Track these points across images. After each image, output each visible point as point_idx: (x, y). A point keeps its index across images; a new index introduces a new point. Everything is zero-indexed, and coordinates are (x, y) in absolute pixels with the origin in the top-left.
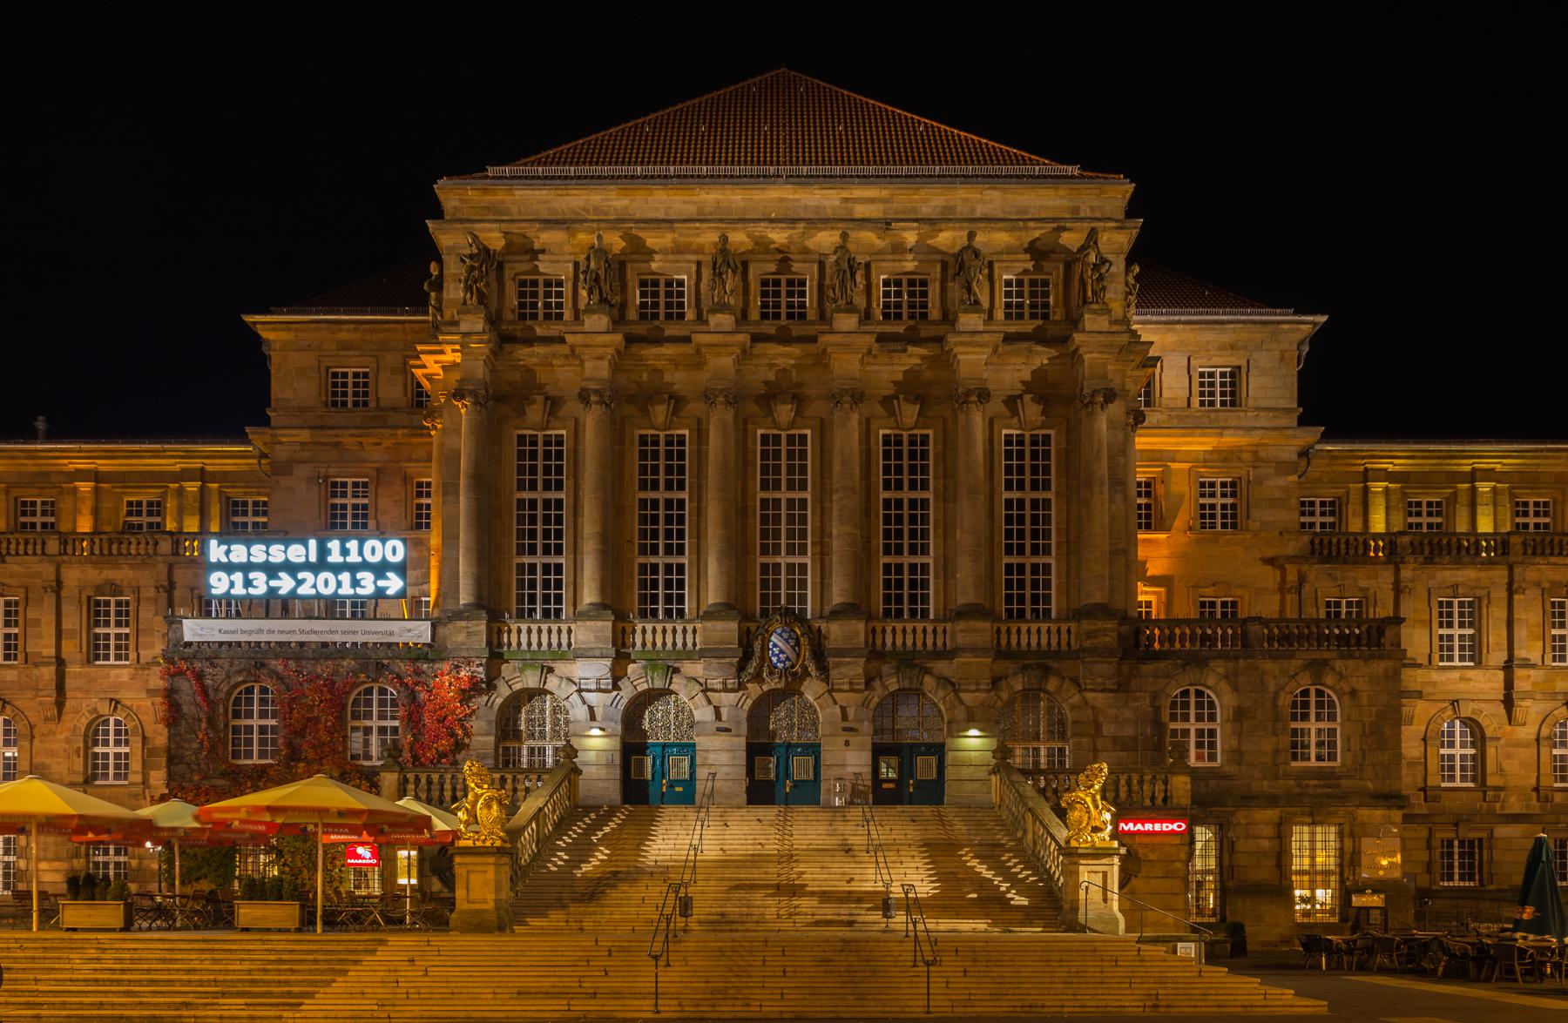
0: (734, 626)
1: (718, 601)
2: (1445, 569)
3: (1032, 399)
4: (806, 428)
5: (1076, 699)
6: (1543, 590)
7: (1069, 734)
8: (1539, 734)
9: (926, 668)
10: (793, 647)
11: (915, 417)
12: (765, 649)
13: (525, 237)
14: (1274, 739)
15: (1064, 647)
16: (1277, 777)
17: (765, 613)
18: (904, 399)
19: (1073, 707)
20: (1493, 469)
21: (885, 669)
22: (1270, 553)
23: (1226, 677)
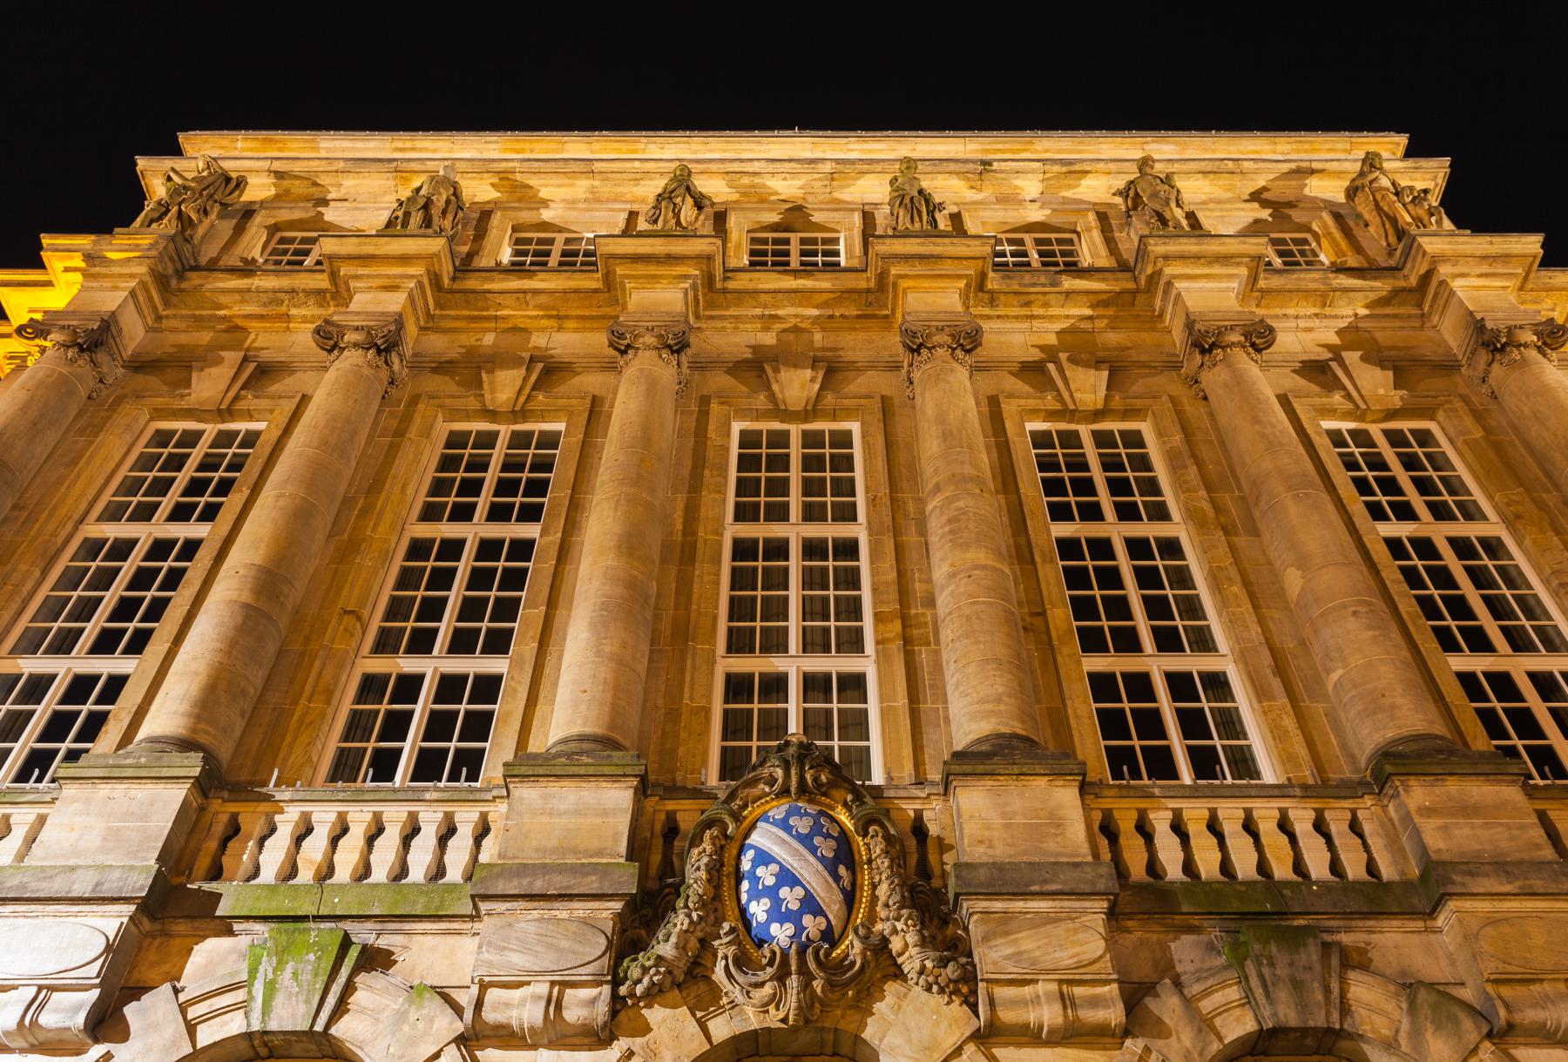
0: (618, 798)
1: (578, 729)
3: (1363, 359)
4: (848, 414)
9: (1344, 951)
10: (831, 866)
11: (1102, 392)
12: (725, 874)
13: (316, 184)
17: (733, 765)
18: (1069, 360)
21: (1185, 951)
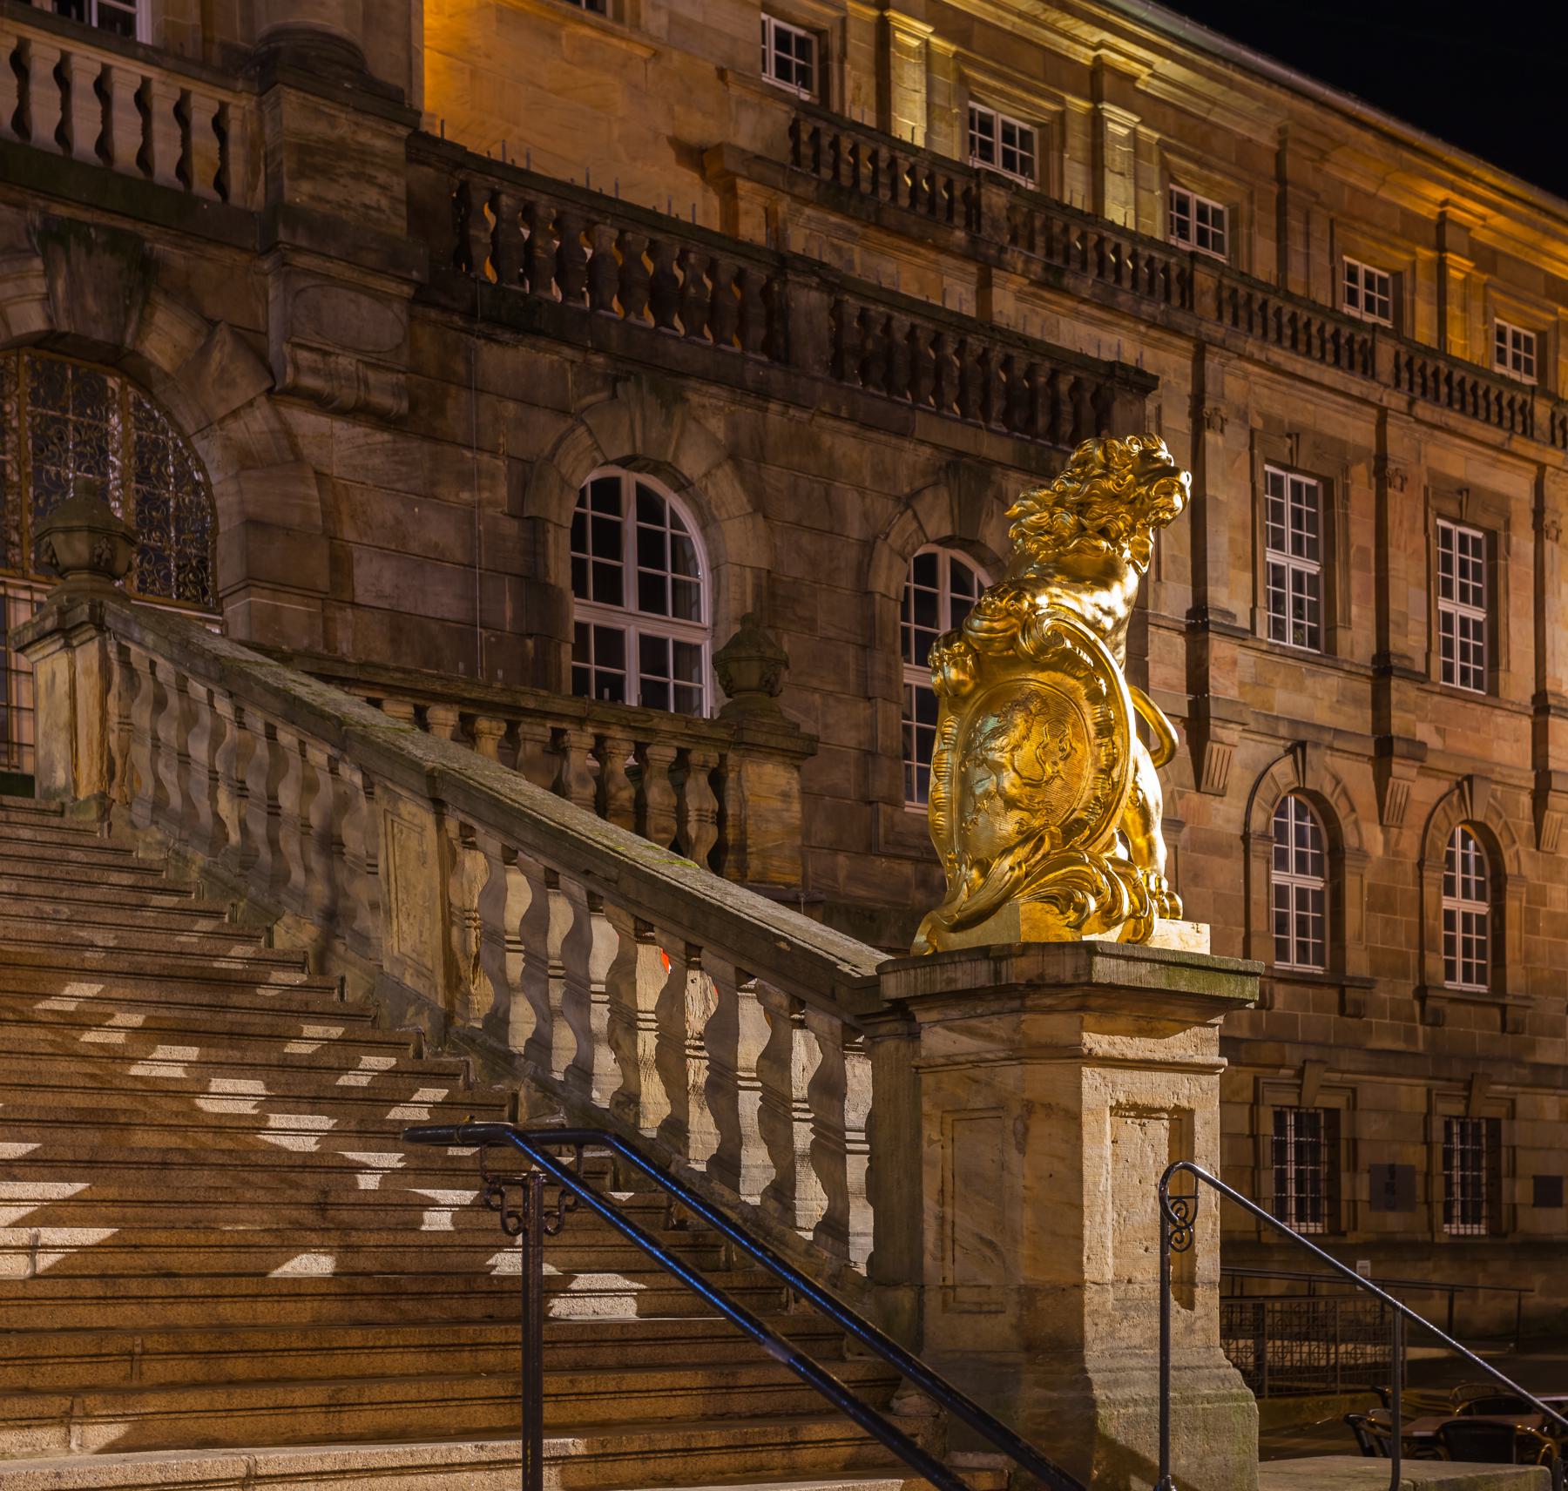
2: (1078, 315)
5: (257, 425)
6: (1252, 432)
7: (227, 570)
8: (1247, 824)
14: (862, 710)
15: (202, 185)
16: (870, 848)
19: (245, 461)
20: (1133, 78)
22: (699, 129)
23: (733, 456)
